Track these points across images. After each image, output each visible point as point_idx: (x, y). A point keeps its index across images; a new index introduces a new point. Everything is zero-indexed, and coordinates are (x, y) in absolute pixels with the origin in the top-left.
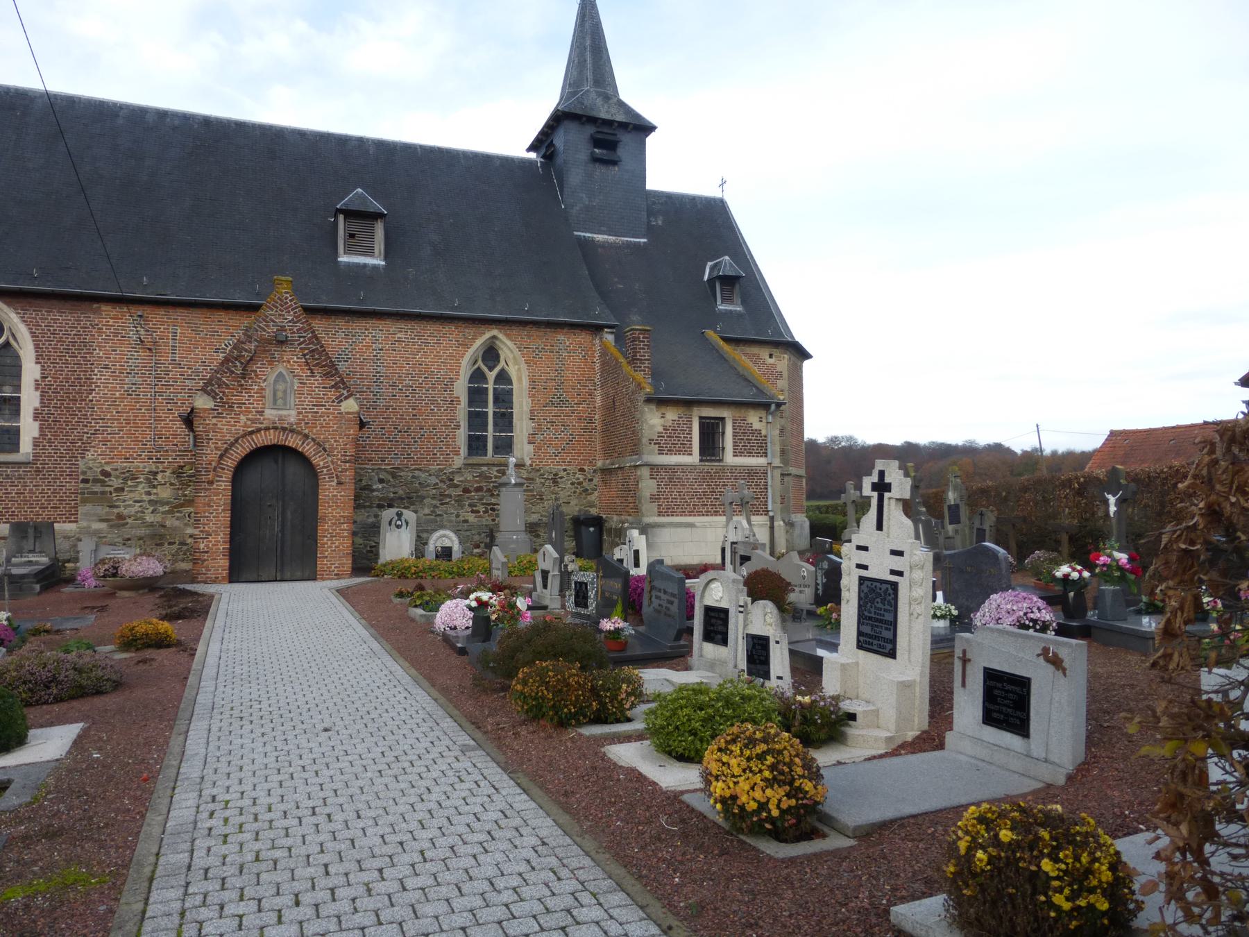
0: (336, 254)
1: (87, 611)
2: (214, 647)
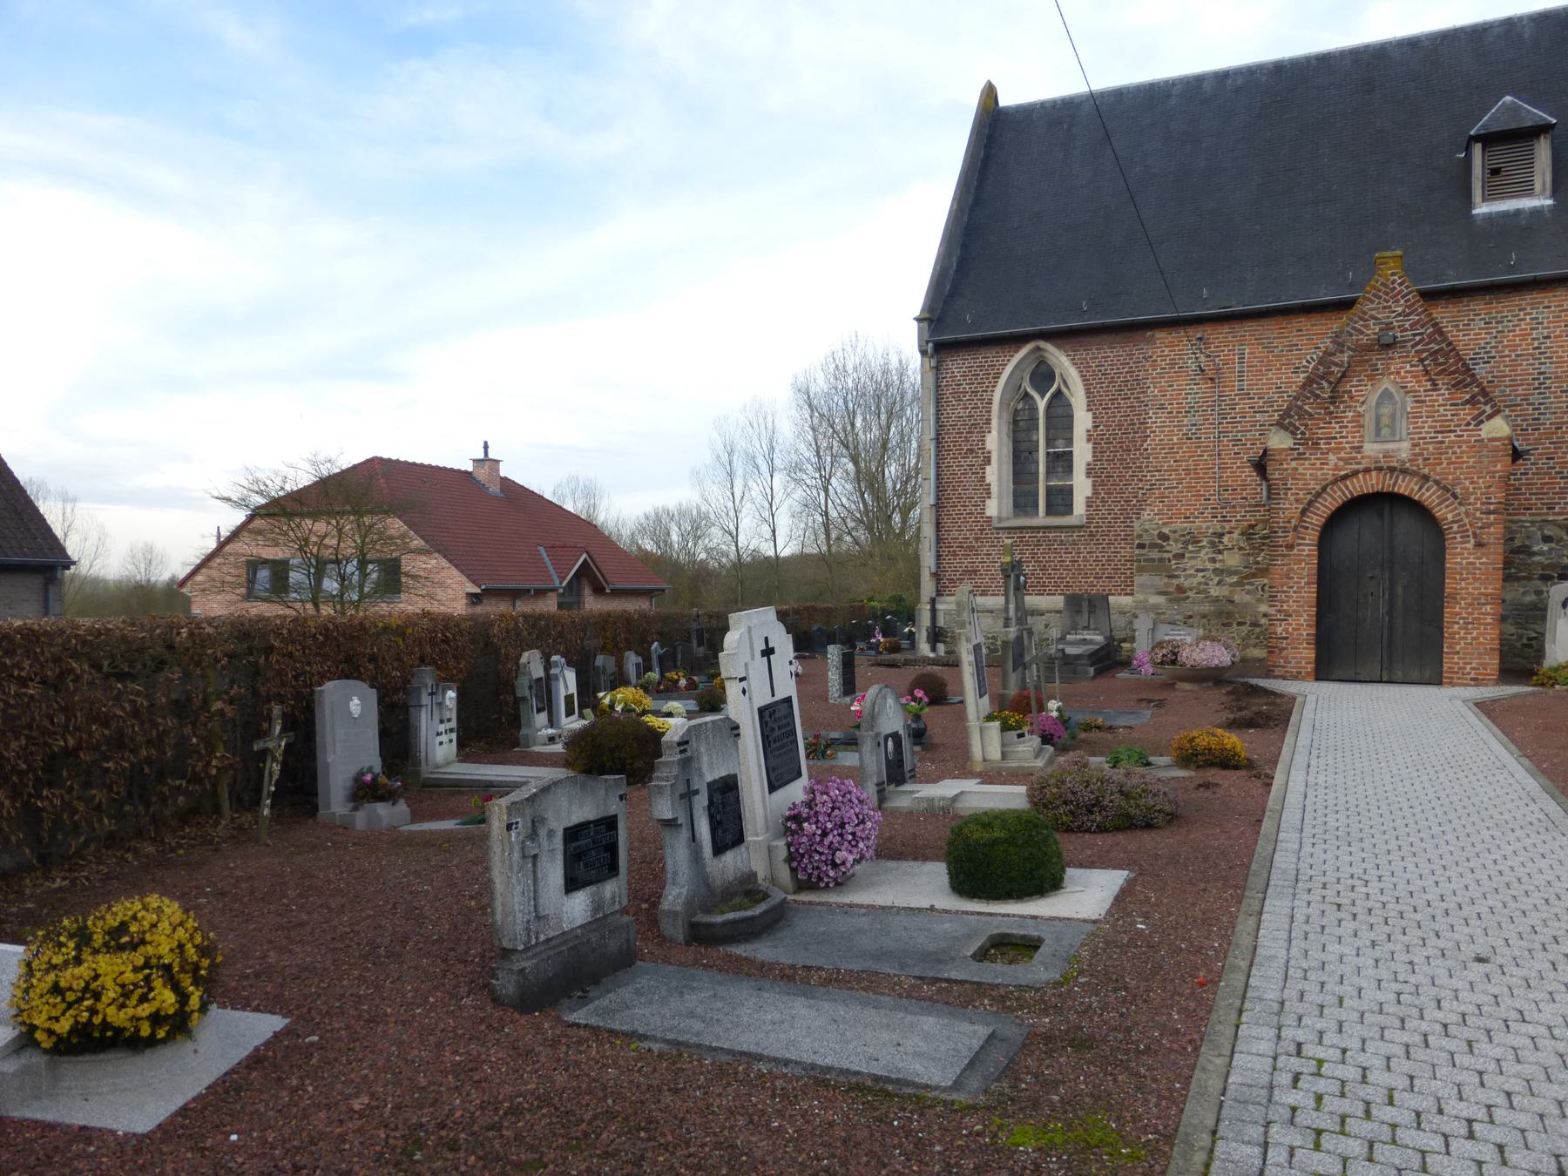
0: (1469, 204)
1: (1143, 704)
2: (1297, 777)
